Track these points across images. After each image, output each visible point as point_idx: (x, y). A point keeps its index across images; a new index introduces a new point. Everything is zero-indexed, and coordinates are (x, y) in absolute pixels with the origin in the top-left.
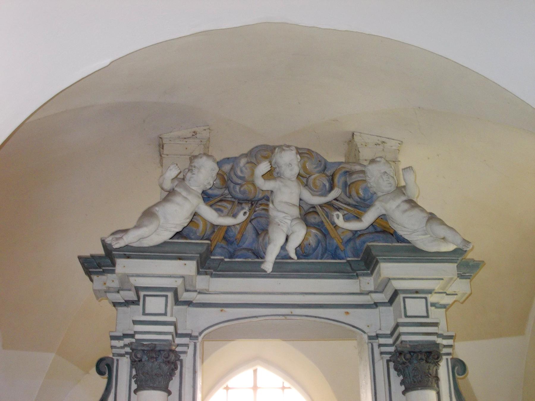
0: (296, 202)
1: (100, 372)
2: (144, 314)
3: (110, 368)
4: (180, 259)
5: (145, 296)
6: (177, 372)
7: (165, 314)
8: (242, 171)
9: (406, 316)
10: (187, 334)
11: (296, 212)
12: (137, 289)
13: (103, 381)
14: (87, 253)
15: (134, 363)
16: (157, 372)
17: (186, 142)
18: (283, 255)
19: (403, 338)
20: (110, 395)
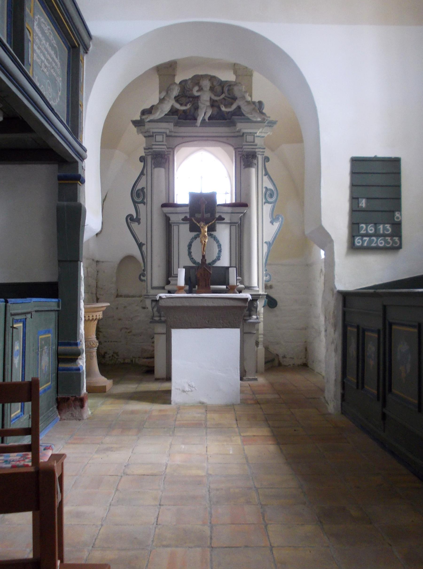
0: (209, 99)
1: (141, 161)
2: (156, 141)
3: (144, 159)
4: (167, 122)
5: (155, 135)
6: (168, 161)
7: (163, 141)
8: (189, 86)
9: (246, 142)
10: (100, 71)
11: (208, 104)
12: (153, 133)
13: (142, 164)
14: (134, 119)
15: (152, 159)
16: (154, 157)
17: (295, 430)
18: (204, 120)
19: (244, 150)
20: (418, 276)
